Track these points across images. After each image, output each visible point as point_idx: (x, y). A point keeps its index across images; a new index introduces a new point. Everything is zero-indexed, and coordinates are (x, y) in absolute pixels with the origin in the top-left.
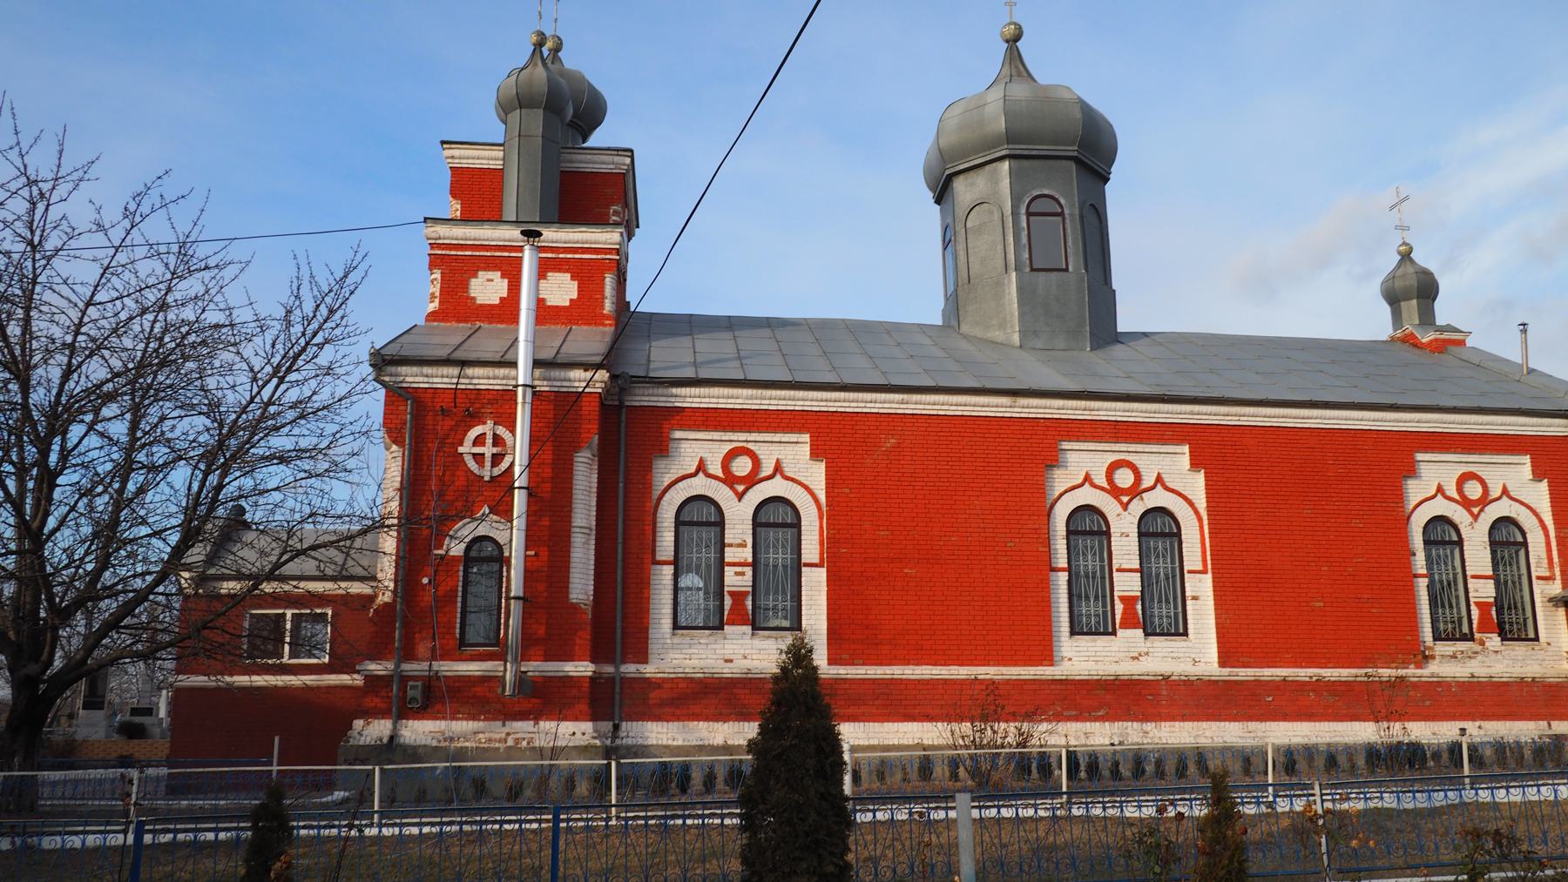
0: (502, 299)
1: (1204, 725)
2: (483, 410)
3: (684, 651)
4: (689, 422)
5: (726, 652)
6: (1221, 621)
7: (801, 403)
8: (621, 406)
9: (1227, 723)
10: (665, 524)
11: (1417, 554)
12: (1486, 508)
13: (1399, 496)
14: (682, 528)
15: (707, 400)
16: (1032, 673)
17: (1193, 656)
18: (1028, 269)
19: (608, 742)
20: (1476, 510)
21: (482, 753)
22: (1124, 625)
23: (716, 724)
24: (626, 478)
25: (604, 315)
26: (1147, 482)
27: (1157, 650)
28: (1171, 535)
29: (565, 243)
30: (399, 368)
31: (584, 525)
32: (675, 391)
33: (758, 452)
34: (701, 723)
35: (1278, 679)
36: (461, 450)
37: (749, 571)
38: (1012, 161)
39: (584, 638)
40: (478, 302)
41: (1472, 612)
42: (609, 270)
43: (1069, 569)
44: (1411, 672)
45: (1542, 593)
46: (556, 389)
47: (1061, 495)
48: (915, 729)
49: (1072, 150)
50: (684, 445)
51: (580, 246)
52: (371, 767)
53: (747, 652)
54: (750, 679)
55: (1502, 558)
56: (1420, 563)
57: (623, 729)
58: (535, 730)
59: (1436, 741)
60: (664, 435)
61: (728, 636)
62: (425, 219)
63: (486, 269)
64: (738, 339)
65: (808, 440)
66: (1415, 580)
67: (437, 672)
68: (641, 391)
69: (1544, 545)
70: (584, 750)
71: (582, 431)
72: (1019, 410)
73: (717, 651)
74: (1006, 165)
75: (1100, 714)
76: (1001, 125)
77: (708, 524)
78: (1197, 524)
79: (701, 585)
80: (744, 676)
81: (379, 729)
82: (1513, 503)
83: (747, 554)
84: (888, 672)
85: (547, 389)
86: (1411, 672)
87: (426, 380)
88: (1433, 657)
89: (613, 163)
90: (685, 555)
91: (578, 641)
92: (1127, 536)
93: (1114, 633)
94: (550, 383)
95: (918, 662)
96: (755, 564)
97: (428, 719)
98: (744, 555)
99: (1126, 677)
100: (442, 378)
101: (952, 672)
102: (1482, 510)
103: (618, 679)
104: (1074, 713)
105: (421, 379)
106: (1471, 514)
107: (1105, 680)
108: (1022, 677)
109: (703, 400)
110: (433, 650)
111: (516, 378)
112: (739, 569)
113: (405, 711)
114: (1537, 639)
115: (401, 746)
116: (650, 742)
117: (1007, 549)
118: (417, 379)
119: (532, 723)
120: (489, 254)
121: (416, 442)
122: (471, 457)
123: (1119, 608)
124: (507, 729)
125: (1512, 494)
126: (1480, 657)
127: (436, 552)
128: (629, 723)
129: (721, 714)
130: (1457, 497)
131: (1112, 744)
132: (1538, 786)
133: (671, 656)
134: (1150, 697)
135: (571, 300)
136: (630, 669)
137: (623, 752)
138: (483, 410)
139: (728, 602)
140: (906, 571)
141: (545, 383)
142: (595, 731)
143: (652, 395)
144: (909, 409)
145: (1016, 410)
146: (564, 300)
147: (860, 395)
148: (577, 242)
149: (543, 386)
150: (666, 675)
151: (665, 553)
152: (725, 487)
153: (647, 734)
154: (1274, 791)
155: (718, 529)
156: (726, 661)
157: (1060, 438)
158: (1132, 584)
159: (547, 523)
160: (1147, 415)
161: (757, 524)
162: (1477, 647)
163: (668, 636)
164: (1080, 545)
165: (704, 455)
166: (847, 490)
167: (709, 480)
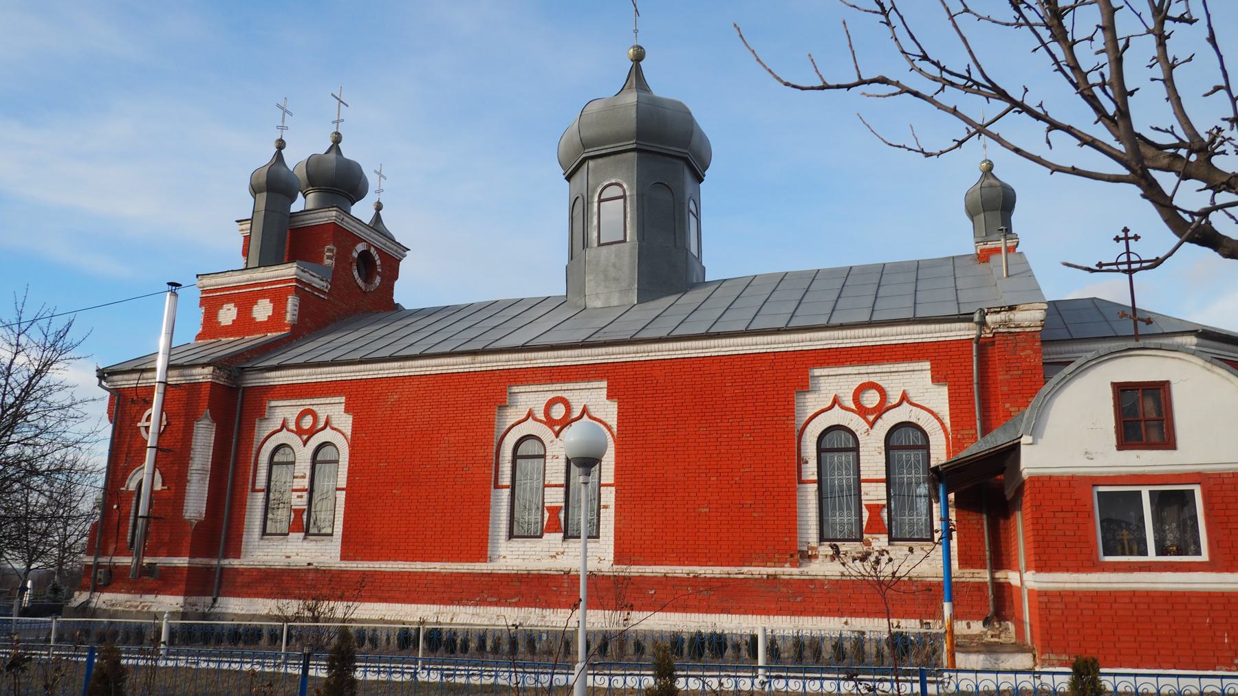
0: (234, 321)
5: (288, 551)
11: (809, 462)
12: (884, 416)
13: (789, 410)
14: (823, 455)
16: (465, 567)
17: (598, 555)
18: (596, 245)
19: (206, 610)
20: (871, 418)
21: (126, 614)
25: (285, 324)
26: (576, 414)
32: (268, 374)
35: (659, 575)
37: (305, 495)
41: (864, 515)
44: (787, 571)
49: (631, 144)
50: (278, 410)
53: (300, 551)
56: (810, 471)
62: (197, 276)
63: (228, 303)
65: (929, 367)
69: (945, 447)
72: (479, 365)
75: (514, 600)
76: (632, 125)
81: (80, 598)
83: (305, 483)
85: (184, 382)
86: (787, 571)
88: (816, 557)
95: (388, 558)
96: (311, 491)
99: (536, 572)
104: (494, 599)
105: (124, 383)
107: (522, 574)
110: (116, 549)
111: (155, 378)
112: (299, 493)
113: (97, 588)
119: (154, 596)
121: (981, 377)
123: (866, 514)
124: (141, 600)
125: (914, 400)
127: (122, 489)
130: (853, 407)
136: (226, 562)
137: (213, 617)
139: (866, 514)
141: (182, 378)
144: (477, 367)
149: (171, 381)
155: (855, 453)
157: (508, 384)
158: (557, 496)
160: (573, 359)
163: (257, 540)
164: (912, 459)
165: (287, 416)
166: (364, 435)
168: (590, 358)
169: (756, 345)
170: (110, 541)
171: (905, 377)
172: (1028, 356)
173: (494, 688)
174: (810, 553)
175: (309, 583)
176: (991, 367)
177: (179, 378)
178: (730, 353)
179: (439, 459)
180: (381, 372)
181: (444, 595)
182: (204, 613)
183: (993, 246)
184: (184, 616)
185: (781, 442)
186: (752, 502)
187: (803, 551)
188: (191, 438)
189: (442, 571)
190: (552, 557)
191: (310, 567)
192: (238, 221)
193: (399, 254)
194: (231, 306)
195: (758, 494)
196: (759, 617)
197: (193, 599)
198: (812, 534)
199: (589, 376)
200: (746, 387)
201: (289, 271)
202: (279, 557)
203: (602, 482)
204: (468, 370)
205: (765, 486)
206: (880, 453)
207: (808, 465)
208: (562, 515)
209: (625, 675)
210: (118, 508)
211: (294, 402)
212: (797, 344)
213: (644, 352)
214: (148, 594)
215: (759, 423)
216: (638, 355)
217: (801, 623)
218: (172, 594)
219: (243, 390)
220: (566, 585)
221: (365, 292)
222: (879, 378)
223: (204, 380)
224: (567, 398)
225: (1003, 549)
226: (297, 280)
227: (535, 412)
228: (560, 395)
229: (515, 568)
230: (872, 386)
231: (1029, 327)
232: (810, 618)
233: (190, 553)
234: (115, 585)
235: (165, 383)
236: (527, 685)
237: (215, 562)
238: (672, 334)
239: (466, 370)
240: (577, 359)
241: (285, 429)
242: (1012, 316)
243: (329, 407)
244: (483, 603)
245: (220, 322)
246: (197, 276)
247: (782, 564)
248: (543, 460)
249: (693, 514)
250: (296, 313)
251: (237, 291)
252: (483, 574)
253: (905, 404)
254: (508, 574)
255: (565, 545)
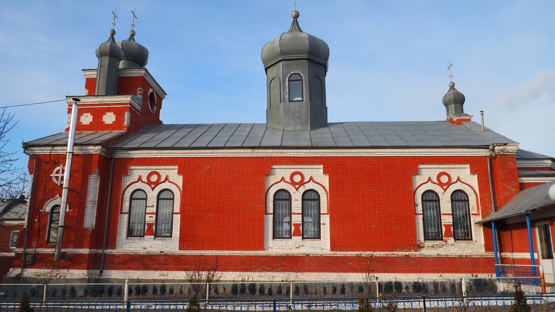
1: (322, 274)
2: (60, 161)
3: (129, 245)
4: (136, 163)
5: (144, 245)
6: (332, 233)
7: (175, 155)
8: (111, 158)
9: (331, 273)
10: (126, 200)
12: (450, 187)
15: (142, 155)
17: (321, 247)
18: (288, 101)
19: (97, 277)
20: (445, 187)
22: (446, 235)
23: (136, 271)
24: (112, 184)
27: (306, 244)
28: (465, 201)
29: (112, 102)
30: (33, 148)
31: (91, 200)
32: (130, 152)
33: (160, 173)
34: (131, 271)
36: (51, 175)
37: (154, 216)
38: (284, 62)
39: (87, 240)
40: (83, 124)
42: (126, 110)
43: (423, 214)
44: (412, 253)
45: (474, 220)
46: (84, 153)
47: (272, 186)
48: (354, 275)
49: (306, 56)
50: (135, 171)
51: (117, 103)
52: (42, 285)
54: (150, 255)
55: (459, 206)
56: (419, 209)
57: (104, 273)
58: (67, 273)
59: (408, 281)
60: (127, 168)
61: (145, 240)
62: (67, 97)
64: (284, 132)
65: (322, 167)
66: (416, 216)
67: (38, 252)
68: (119, 153)
70: (82, 280)
71: (92, 167)
72: (256, 154)
73: (141, 245)
74: (281, 63)
75: (280, 269)
76: (307, 48)
77: (314, 200)
78: (326, 195)
79: (312, 220)
80: (147, 254)
81: (18, 271)
82: (462, 184)
83: (155, 210)
84: (199, 253)
85: (81, 153)
86: (412, 253)
87: (42, 152)
88: (424, 247)
89: (139, 73)
90: (277, 211)
91: (85, 242)
92: (298, 200)
93: (291, 238)
94: (82, 151)
96: (157, 214)
97: (33, 268)
98: (153, 210)
99: (291, 255)
100: (46, 151)
101: (223, 253)
102: (448, 187)
103: (103, 255)
104: (270, 269)
105: (40, 151)
106: (443, 189)
108: (250, 255)
109: (141, 155)
110: (38, 244)
111: (67, 150)
113: (26, 266)
114: (472, 239)
115: (22, 277)
116: (112, 277)
117: (248, 206)
118: (39, 152)
119: (67, 270)
120: (87, 107)
122: (55, 177)
123: (146, 227)
125: (462, 180)
126: (444, 247)
127: (41, 211)
128: (106, 270)
129: (138, 267)
130: (437, 182)
131: (283, 281)
132: (411, 302)
133: (125, 246)
134: (301, 263)
135: (113, 122)
136: (108, 251)
138: (60, 161)
139: (146, 227)
140: (210, 215)
141: (81, 151)
142: (88, 273)
143: (123, 154)
144: (214, 155)
145: (255, 154)
146: (111, 122)
147: (196, 151)
148: (116, 102)
149: (75, 152)
150: (120, 253)
151: (125, 210)
152: (148, 185)
153: (111, 274)
154: (292, 302)
155: (318, 202)
156: (144, 248)
157: (272, 164)
159: (78, 200)
160: (306, 154)
161: (158, 199)
162: (444, 243)
163: (125, 239)
166: (190, 186)
167: (142, 183)
168: (315, 154)
169: (395, 153)
170: (33, 239)
171: (458, 170)
172: (511, 165)
173: (489, 308)
174: (421, 245)
175: (161, 261)
176: (494, 168)
177: (78, 151)
178: (382, 156)
179: (235, 199)
180: (199, 154)
181: (241, 267)
182: (96, 279)
183: (463, 118)
184: (89, 281)
185: (407, 196)
186: (396, 223)
187: (418, 245)
188: (88, 184)
189: (240, 255)
190: (297, 248)
191: (162, 253)
192: (83, 70)
193: (163, 96)
194: (89, 114)
195: (398, 219)
196: (402, 274)
197: (91, 271)
198: (421, 236)
199: (313, 162)
200: (390, 171)
201: (126, 99)
202: (139, 248)
203: (147, 212)
204: (249, 156)
205: (401, 215)
206: (449, 203)
207: (418, 207)
208: (154, 227)
209: (438, 301)
210: (38, 221)
211: (145, 167)
212: (413, 154)
213: (342, 153)
214: (62, 269)
215: (396, 188)
216: (338, 154)
217: (421, 276)
218: (79, 269)
219: (114, 160)
220: (307, 261)
221: (151, 113)
222: (447, 171)
223: (95, 153)
224: (302, 172)
225: (503, 243)
226: (130, 104)
227: (285, 178)
228: (297, 171)
229: (281, 253)
230: (445, 173)
231: (512, 152)
232: (425, 274)
233: (89, 246)
234: (38, 264)
235: (73, 153)
236: (296, 309)
237: (100, 251)
238: (190, 146)
239: (248, 156)
240: (308, 154)
241: (140, 181)
242: (506, 148)
243: (167, 171)
244: (263, 270)
245: (82, 123)
246: (67, 97)
247: (410, 250)
248: (145, 201)
249: (368, 228)
250: (129, 121)
251: (92, 107)
252: (262, 256)
253: (458, 182)
254: (276, 256)
255: (304, 242)
